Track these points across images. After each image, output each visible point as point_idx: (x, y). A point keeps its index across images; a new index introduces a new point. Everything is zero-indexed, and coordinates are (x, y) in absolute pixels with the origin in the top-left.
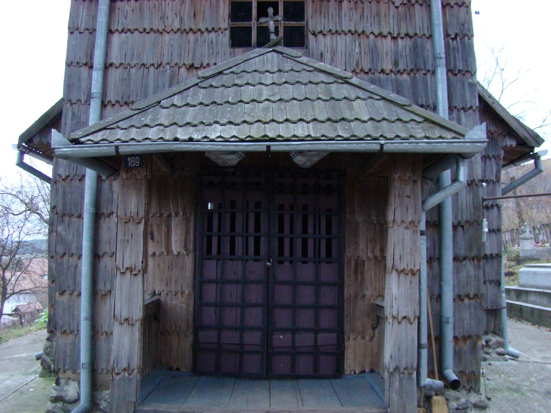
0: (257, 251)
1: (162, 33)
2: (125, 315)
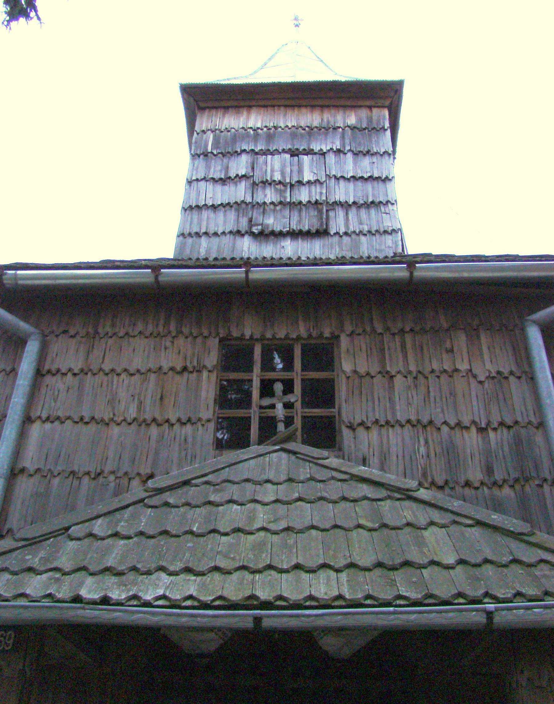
1: (108, 424)
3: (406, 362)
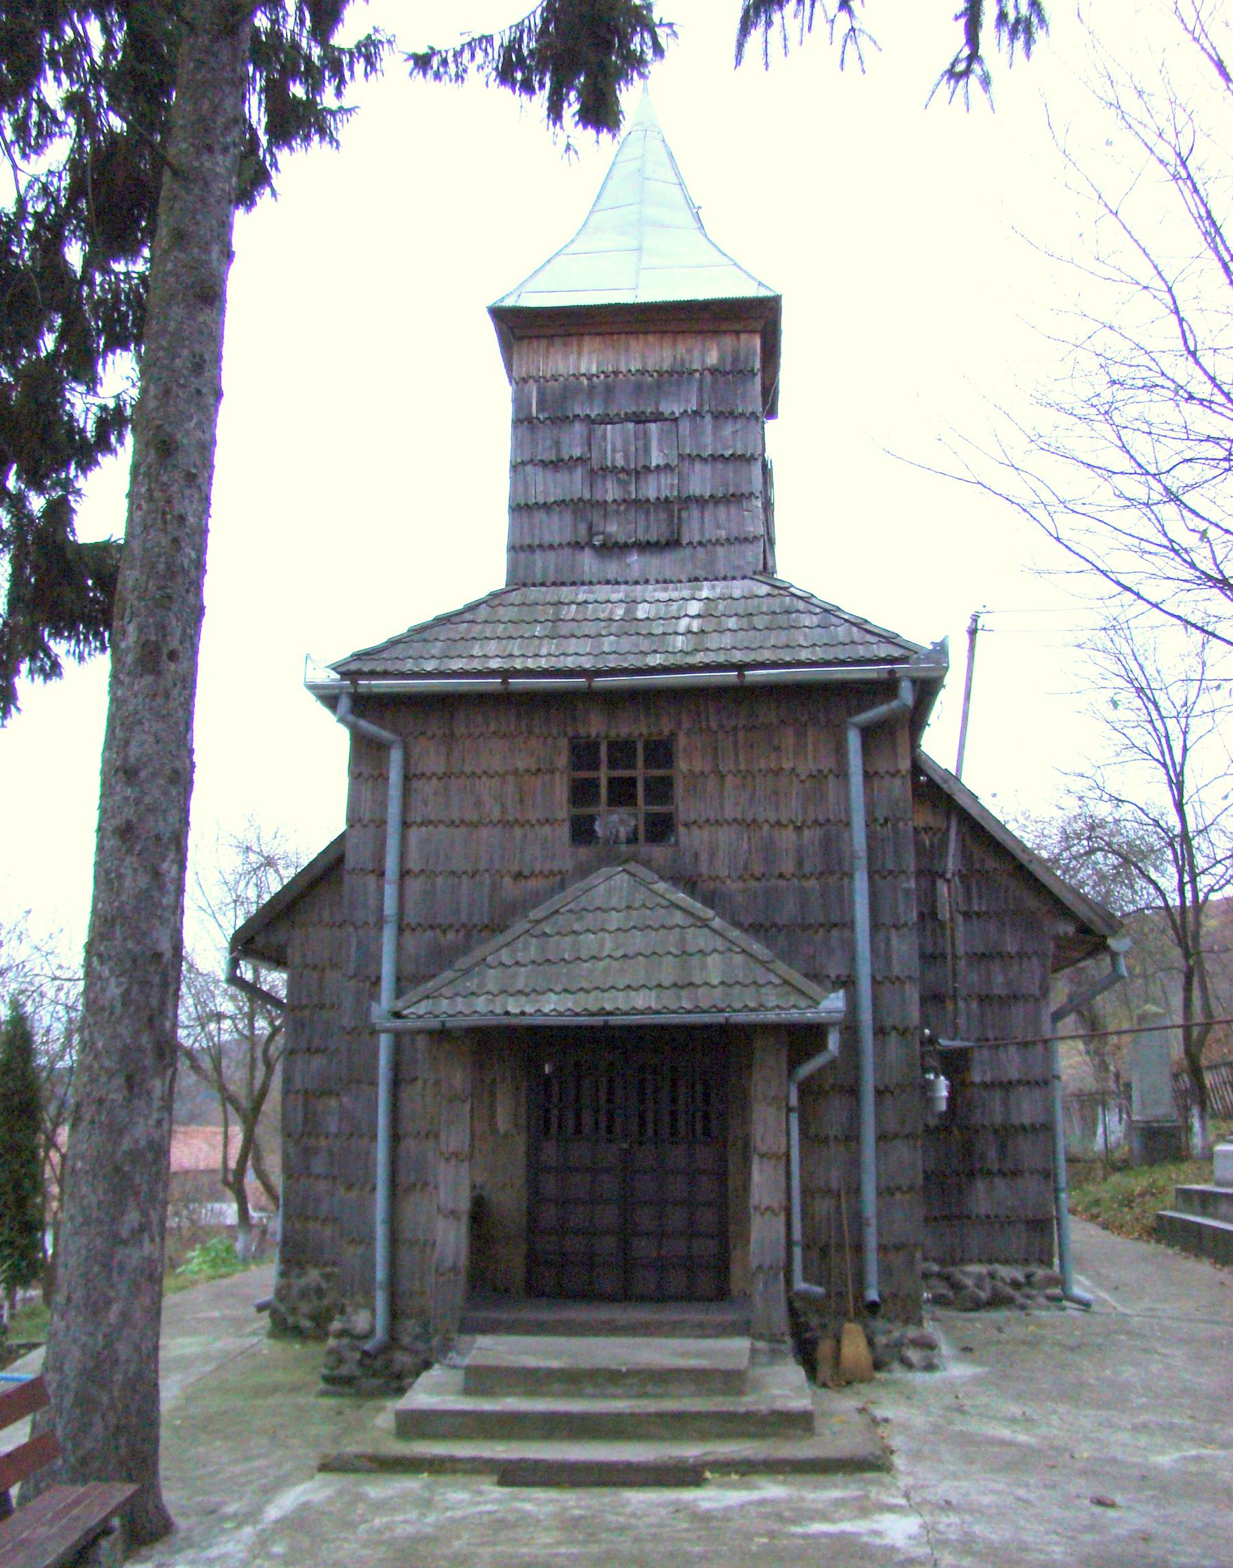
0: (610, 1130)
2: (450, 1206)
3: (737, 762)
